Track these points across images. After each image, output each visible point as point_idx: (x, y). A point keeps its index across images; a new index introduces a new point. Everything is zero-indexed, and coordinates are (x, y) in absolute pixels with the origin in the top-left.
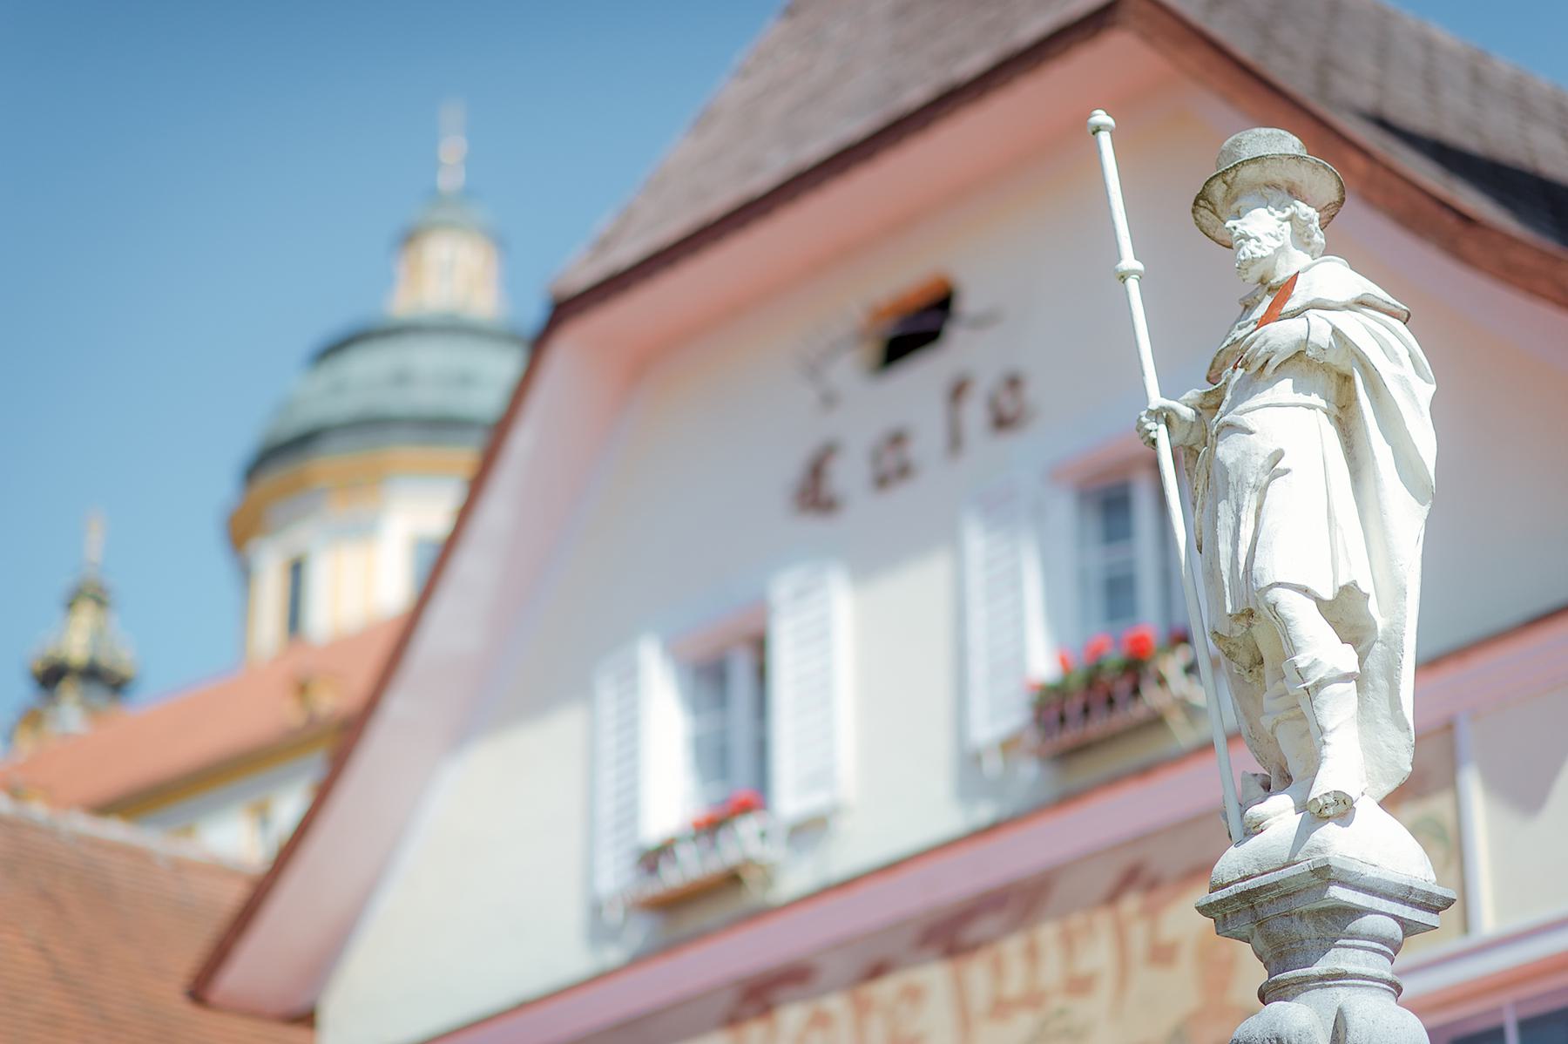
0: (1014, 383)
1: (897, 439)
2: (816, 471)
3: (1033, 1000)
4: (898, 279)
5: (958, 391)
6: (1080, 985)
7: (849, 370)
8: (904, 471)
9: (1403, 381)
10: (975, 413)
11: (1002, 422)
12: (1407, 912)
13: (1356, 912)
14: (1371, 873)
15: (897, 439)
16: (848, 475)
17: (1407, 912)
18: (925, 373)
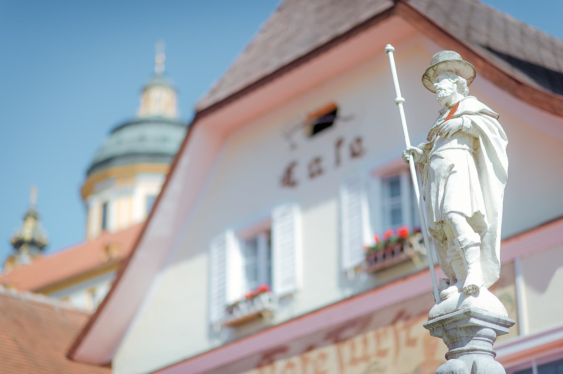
0: (359, 141)
1: (317, 160)
2: (289, 172)
3: (365, 358)
4: (317, 104)
5: (339, 143)
6: (382, 353)
7: (300, 136)
8: (320, 172)
9: (496, 140)
10: (345, 151)
11: (355, 155)
12: (498, 327)
13: (479, 328)
14: (485, 314)
15: (317, 160)
16: (300, 173)
17: (498, 327)
18: (327, 138)
